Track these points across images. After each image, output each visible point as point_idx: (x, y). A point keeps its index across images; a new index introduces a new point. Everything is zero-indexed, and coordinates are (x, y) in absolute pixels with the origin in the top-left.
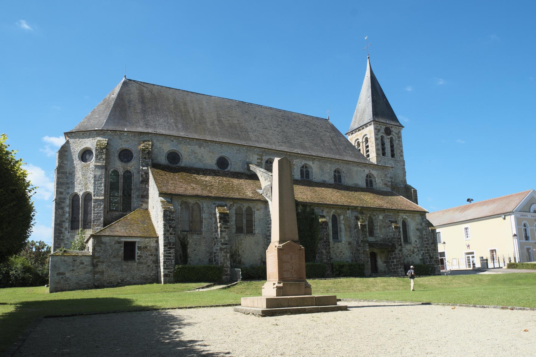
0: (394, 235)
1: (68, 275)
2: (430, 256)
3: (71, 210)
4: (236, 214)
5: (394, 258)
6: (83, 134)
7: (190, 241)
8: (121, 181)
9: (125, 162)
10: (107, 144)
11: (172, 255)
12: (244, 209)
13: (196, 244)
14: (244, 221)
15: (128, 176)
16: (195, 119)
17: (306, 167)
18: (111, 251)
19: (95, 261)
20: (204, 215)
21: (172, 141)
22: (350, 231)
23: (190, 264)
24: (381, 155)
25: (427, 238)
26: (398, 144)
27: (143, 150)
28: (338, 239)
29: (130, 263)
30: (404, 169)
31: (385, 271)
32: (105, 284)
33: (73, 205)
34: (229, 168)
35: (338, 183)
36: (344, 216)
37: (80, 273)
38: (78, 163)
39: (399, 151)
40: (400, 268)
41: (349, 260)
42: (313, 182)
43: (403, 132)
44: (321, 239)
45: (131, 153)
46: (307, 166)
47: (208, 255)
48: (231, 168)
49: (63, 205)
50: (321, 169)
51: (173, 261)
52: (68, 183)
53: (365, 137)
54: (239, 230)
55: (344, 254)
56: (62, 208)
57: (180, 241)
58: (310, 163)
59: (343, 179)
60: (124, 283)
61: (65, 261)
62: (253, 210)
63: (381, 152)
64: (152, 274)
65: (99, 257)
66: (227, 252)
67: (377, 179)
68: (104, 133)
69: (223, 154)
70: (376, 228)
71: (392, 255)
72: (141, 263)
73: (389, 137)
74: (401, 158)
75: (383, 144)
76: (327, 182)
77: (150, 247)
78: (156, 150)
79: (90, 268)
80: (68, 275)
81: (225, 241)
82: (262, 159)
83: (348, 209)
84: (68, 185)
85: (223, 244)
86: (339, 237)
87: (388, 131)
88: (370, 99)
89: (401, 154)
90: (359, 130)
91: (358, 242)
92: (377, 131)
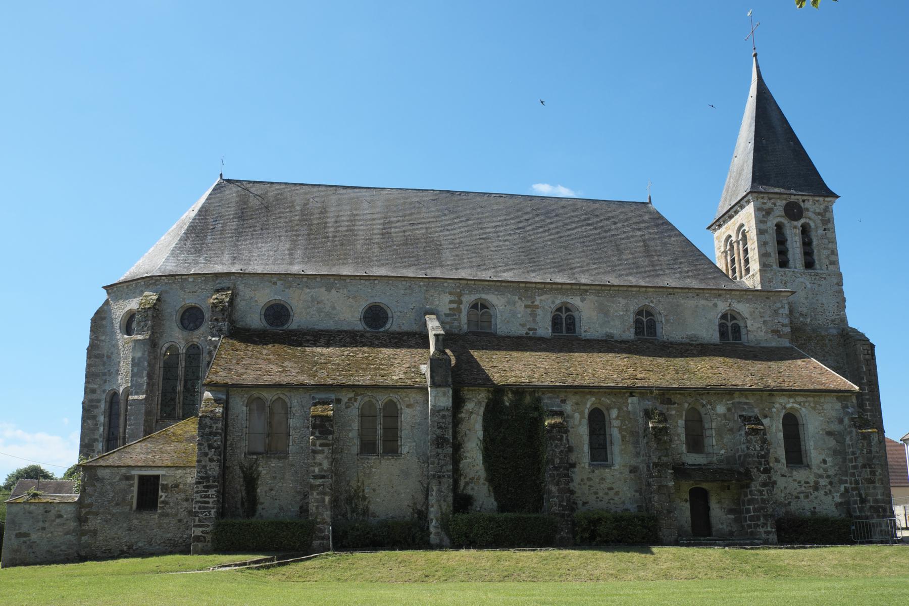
0: (748, 448)
1: (34, 537)
2: (860, 495)
3: (107, 419)
4: (362, 416)
5: (750, 502)
6: (128, 287)
7: (264, 472)
8: (182, 364)
9: (190, 330)
10: (158, 300)
11: (211, 500)
12: (380, 405)
13: (275, 478)
14: (380, 431)
15: (194, 353)
16: (335, 237)
17: (568, 310)
18: (112, 494)
19: (84, 511)
20: (292, 422)
21: (275, 283)
22: (637, 443)
23: (262, 517)
24: (775, 267)
25: (853, 453)
26: (824, 237)
27: (214, 306)
28: (606, 460)
29: (146, 515)
30: (841, 292)
31: (731, 533)
32: (99, 554)
33: (111, 412)
34: (388, 326)
35: (646, 338)
36: (620, 409)
37: (56, 534)
38: (122, 338)
39: (826, 252)
40: (765, 525)
41: (633, 508)
42: (581, 340)
43: (838, 209)
44: (548, 462)
45: (202, 313)
46: (569, 306)
47: (298, 498)
48: (393, 326)
49: (96, 411)
50: (603, 311)
51: (213, 511)
52: (104, 374)
53: (728, 234)
54: (368, 448)
55: (617, 493)
56: (94, 417)
57: (243, 472)
58: (576, 301)
59: (658, 326)
60: (131, 551)
61: (30, 513)
62: (399, 407)
63: (774, 259)
64: (185, 536)
65: (90, 505)
66: (325, 494)
67: (749, 323)
68: (156, 281)
69: (377, 300)
70: (708, 433)
71: (746, 495)
72: (167, 515)
73: (799, 223)
74: (831, 267)
75: (781, 241)
76: (617, 338)
77: (185, 485)
78: (243, 303)
79: (73, 525)
80: (34, 537)
81: (322, 470)
82: (460, 302)
83: (631, 395)
84: (104, 378)
85: (315, 477)
86: (609, 456)
87: (794, 211)
88: (751, 146)
89: (833, 258)
90: (731, 217)
91: (648, 466)
92: (763, 214)
